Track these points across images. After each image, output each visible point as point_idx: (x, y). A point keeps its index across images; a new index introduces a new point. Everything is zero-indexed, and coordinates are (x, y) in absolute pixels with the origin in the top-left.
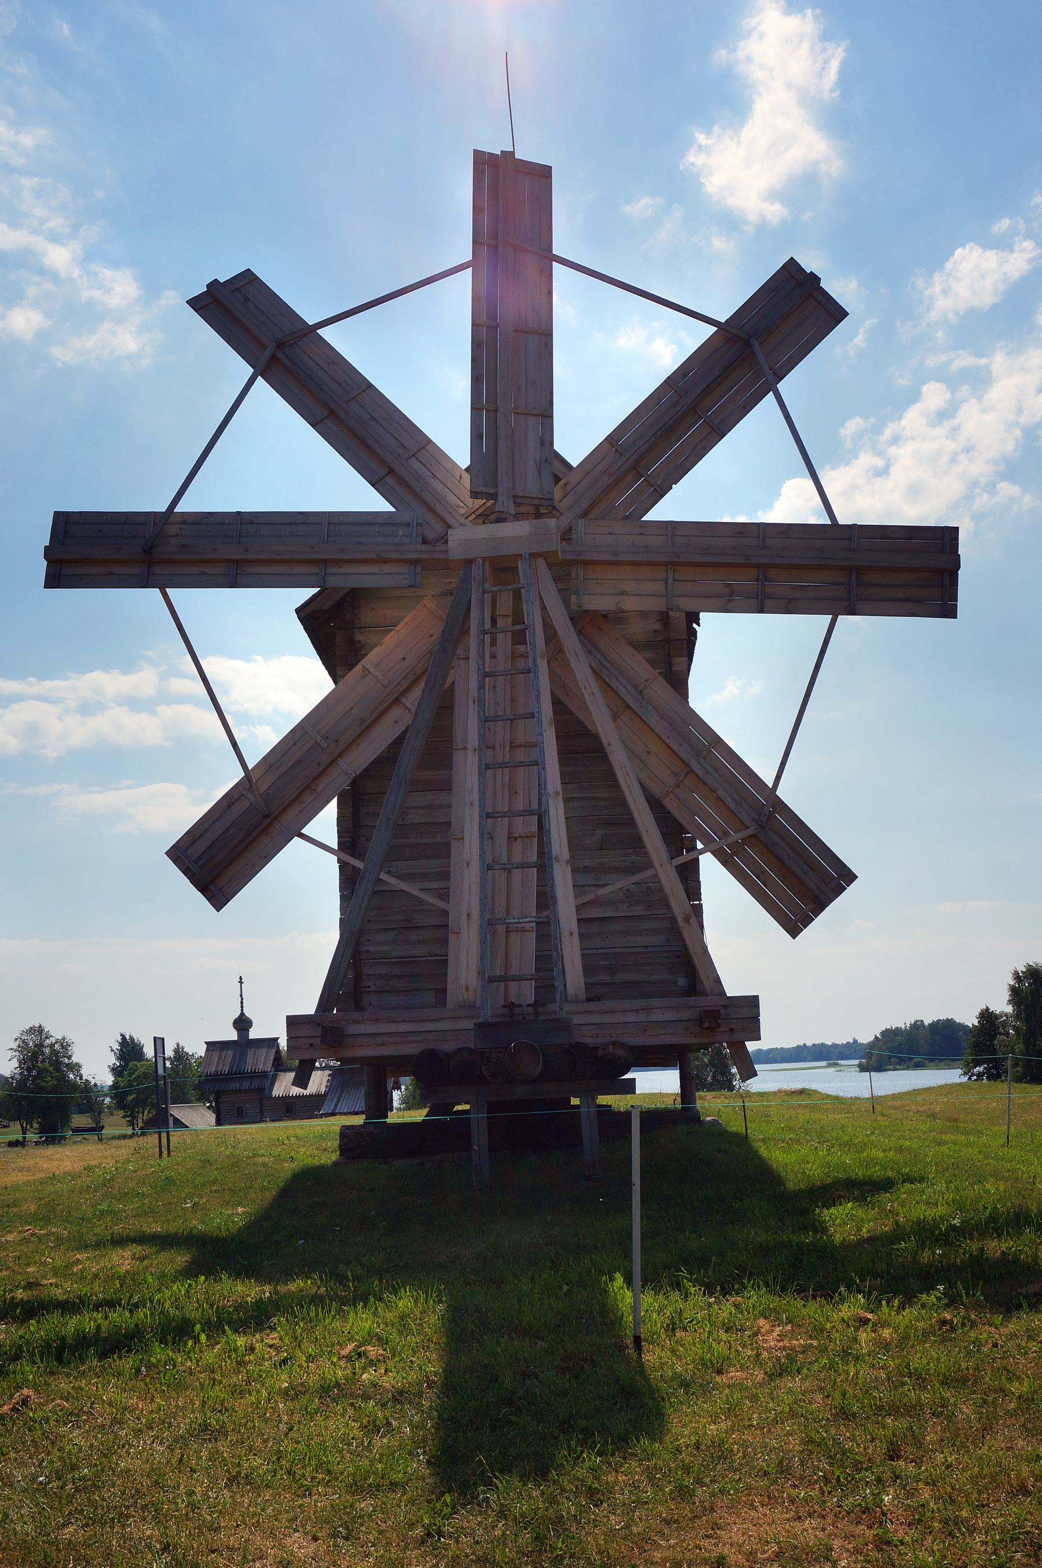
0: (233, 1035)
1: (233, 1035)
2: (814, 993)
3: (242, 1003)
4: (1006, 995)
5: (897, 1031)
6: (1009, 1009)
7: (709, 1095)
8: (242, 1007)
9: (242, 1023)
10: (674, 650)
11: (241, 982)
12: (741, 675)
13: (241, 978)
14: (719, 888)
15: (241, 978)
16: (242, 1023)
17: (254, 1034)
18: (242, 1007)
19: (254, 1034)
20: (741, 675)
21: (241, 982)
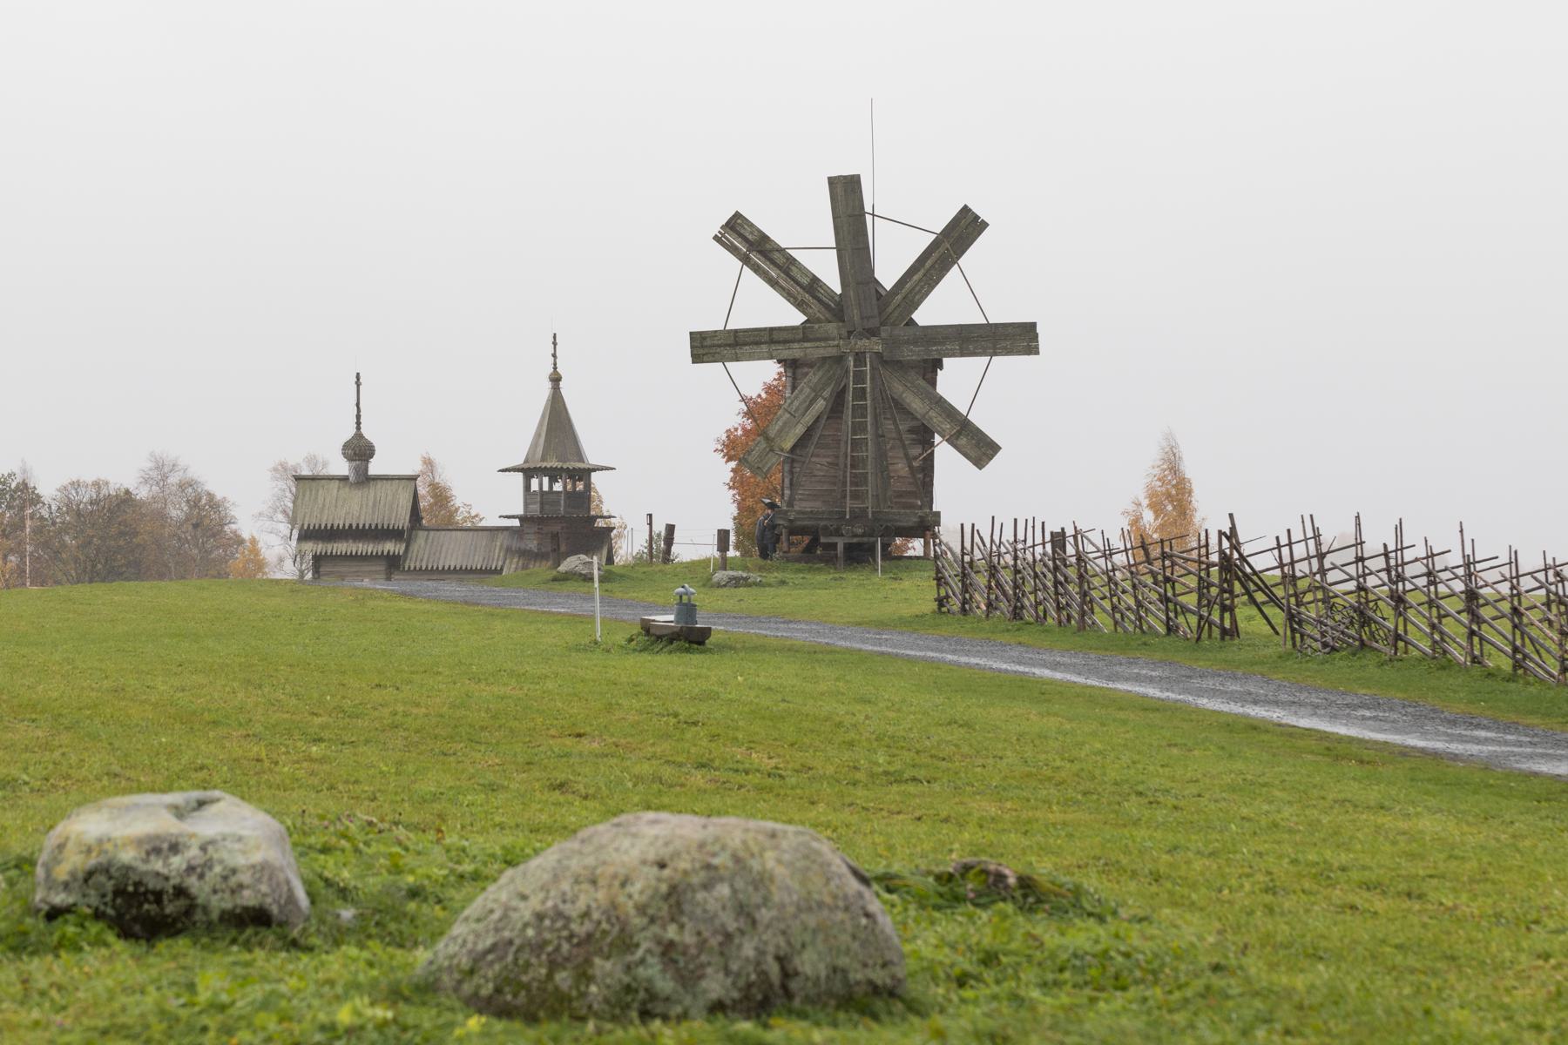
1: (341, 467)
2: (964, 499)
3: (358, 417)
8: (358, 423)
9: (359, 450)
10: (912, 323)
14: (946, 457)
16: (359, 450)
17: (375, 467)
18: (358, 423)
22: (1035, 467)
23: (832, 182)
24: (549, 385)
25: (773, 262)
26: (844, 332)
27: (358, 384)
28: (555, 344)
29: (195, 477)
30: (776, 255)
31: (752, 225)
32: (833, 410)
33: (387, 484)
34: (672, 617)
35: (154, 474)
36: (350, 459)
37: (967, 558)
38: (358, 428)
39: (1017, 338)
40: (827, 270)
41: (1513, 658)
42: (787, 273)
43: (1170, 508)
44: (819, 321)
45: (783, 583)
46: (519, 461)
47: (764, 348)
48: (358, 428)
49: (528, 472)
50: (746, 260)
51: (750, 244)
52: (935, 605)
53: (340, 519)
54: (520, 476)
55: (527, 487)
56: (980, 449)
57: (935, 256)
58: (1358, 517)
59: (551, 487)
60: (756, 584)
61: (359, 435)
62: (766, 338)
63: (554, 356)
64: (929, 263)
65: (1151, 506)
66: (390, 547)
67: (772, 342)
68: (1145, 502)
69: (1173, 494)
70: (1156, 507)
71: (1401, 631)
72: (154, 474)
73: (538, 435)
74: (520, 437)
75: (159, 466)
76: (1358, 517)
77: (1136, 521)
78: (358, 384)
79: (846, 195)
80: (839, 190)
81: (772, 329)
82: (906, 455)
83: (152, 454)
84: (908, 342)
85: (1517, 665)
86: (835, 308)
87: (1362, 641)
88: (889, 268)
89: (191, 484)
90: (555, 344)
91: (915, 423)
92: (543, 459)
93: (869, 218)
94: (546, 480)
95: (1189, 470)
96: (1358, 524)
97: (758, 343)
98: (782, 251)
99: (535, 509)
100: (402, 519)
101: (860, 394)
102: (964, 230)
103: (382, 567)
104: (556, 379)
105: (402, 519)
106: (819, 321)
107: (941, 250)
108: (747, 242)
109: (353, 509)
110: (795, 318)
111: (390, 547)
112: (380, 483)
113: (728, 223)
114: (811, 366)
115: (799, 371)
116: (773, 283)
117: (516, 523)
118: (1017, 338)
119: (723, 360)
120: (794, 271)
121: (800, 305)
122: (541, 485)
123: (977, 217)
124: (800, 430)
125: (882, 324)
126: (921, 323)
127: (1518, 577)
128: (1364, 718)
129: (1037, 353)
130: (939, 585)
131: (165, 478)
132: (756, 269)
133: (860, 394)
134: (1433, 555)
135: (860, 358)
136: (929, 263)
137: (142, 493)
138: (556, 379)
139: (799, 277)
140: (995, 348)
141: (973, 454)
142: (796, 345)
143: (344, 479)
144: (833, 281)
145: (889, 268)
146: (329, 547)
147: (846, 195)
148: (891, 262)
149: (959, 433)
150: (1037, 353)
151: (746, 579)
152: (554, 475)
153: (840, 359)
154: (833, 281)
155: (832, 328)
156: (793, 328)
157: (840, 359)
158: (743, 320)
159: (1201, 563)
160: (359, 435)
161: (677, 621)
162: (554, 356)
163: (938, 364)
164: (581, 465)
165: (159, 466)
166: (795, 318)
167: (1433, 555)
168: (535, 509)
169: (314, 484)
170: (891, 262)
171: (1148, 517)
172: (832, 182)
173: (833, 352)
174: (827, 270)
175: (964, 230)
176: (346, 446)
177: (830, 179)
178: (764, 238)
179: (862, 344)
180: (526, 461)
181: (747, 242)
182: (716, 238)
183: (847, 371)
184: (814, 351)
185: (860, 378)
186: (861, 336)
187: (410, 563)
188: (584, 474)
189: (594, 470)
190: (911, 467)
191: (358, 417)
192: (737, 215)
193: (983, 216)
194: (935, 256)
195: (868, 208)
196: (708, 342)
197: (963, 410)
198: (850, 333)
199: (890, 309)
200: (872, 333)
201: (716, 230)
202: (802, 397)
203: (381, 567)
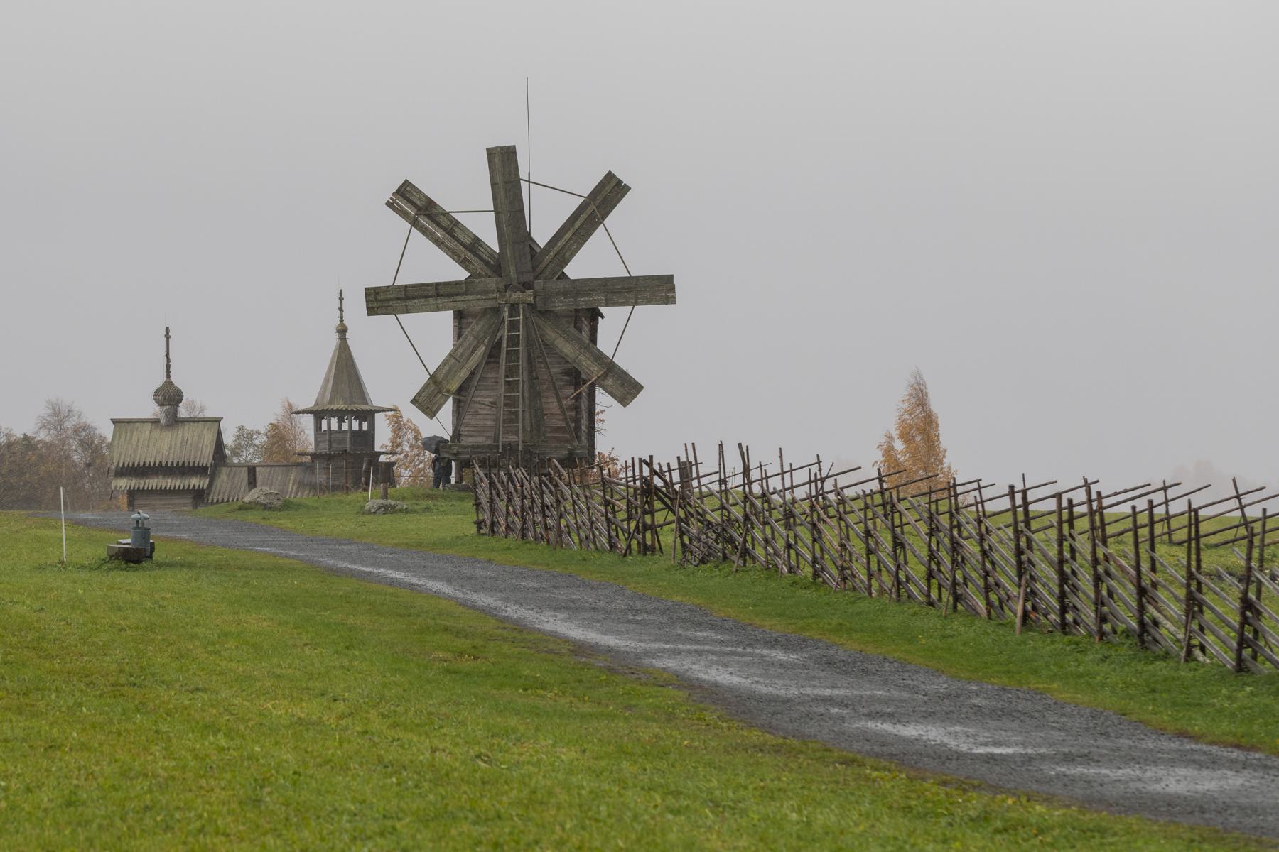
2: (625, 436)
3: (168, 366)
8: (168, 372)
9: (169, 396)
10: (564, 276)
14: (603, 399)
16: (169, 396)
17: (183, 412)
18: (168, 372)
22: (672, 405)
23: (490, 152)
24: (337, 336)
25: (438, 224)
26: (502, 285)
27: (168, 337)
28: (341, 299)
29: (89, 422)
30: (441, 219)
31: (420, 192)
32: (490, 356)
33: (194, 427)
34: (129, 541)
35: (52, 419)
36: (161, 404)
37: (756, 489)
38: (168, 376)
39: (658, 289)
40: (486, 230)
41: (813, 566)
42: (450, 233)
43: (918, 439)
44: (480, 276)
45: (428, 509)
46: (310, 403)
47: (431, 300)
48: (168, 376)
50: (415, 223)
51: (419, 210)
52: (474, 529)
53: (151, 458)
54: (311, 417)
55: (318, 427)
56: (627, 389)
57: (583, 217)
58: (721, 445)
59: (340, 427)
60: (407, 511)
61: (168, 384)
62: (432, 292)
63: (341, 309)
64: (577, 225)
65: (901, 436)
66: (195, 482)
67: (438, 295)
68: (895, 434)
69: (921, 428)
70: (906, 436)
71: (749, 546)
72: (52, 419)
73: (327, 380)
74: (308, 384)
75: (56, 413)
76: (721, 445)
77: (888, 451)
78: (168, 337)
79: (503, 162)
80: (497, 160)
81: (438, 284)
82: (557, 394)
83: (49, 402)
84: (558, 294)
85: (816, 575)
86: (496, 266)
87: (724, 554)
88: (543, 228)
89: (85, 428)
90: (341, 299)
91: (569, 366)
92: (331, 402)
93: (524, 185)
94: (334, 421)
95: (936, 406)
96: (721, 452)
97: (426, 297)
98: (446, 214)
99: (324, 446)
100: (206, 457)
101: (514, 341)
102: (609, 193)
103: (188, 500)
104: (342, 331)
105: (206, 457)
106: (480, 276)
107: (589, 211)
108: (415, 206)
109: (164, 447)
110: (460, 274)
111: (195, 482)
112: (187, 425)
113: (398, 191)
114: (474, 316)
115: (464, 321)
116: (439, 243)
117: (307, 459)
118: (658, 289)
119: (394, 311)
120: (458, 233)
121: (464, 263)
122: (350, 426)
123: (620, 182)
124: (464, 374)
125: (537, 278)
127: (982, 502)
128: (644, 624)
129: (674, 302)
130: (477, 510)
131: (61, 423)
132: (424, 231)
133: (514, 341)
134: (767, 477)
135: (514, 308)
136: (577, 225)
137: (42, 436)
138: (342, 331)
139: (462, 237)
140: (636, 298)
141: (617, 393)
142: (459, 298)
143: (155, 422)
144: (491, 240)
145: (543, 228)
146: (142, 482)
147: (503, 162)
148: (543, 224)
149: (605, 376)
150: (674, 302)
151: (394, 507)
152: (341, 415)
153: (496, 311)
154: (491, 240)
155: (492, 283)
156: (457, 283)
157: (496, 311)
158: (412, 276)
159: (628, 487)
160: (168, 384)
161: (134, 542)
162: (341, 309)
163: (595, 315)
164: (364, 407)
165: (56, 413)
166: (460, 274)
167: (767, 477)
168: (324, 446)
169: (129, 427)
170: (543, 224)
171: (899, 446)
172: (490, 152)
173: (489, 304)
174: (486, 230)
175: (609, 193)
176: (157, 393)
177: (488, 150)
178: (431, 203)
179: (515, 296)
180: (316, 404)
181: (415, 206)
182: (388, 204)
183: (503, 321)
184: (475, 304)
185: (513, 326)
186: (515, 289)
187: (214, 497)
188: (368, 415)
189: (379, 411)
190: (561, 406)
191: (168, 366)
192: (407, 183)
193: (626, 181)
194: (583, 217)
195: (523, 174)
196: (381, 297)
197: (609, 353)
198: (507, 287)
199: (543, 265)
200: (527, 286)
201: (388, 196)
202: (466, 344)
203: (188, 500)
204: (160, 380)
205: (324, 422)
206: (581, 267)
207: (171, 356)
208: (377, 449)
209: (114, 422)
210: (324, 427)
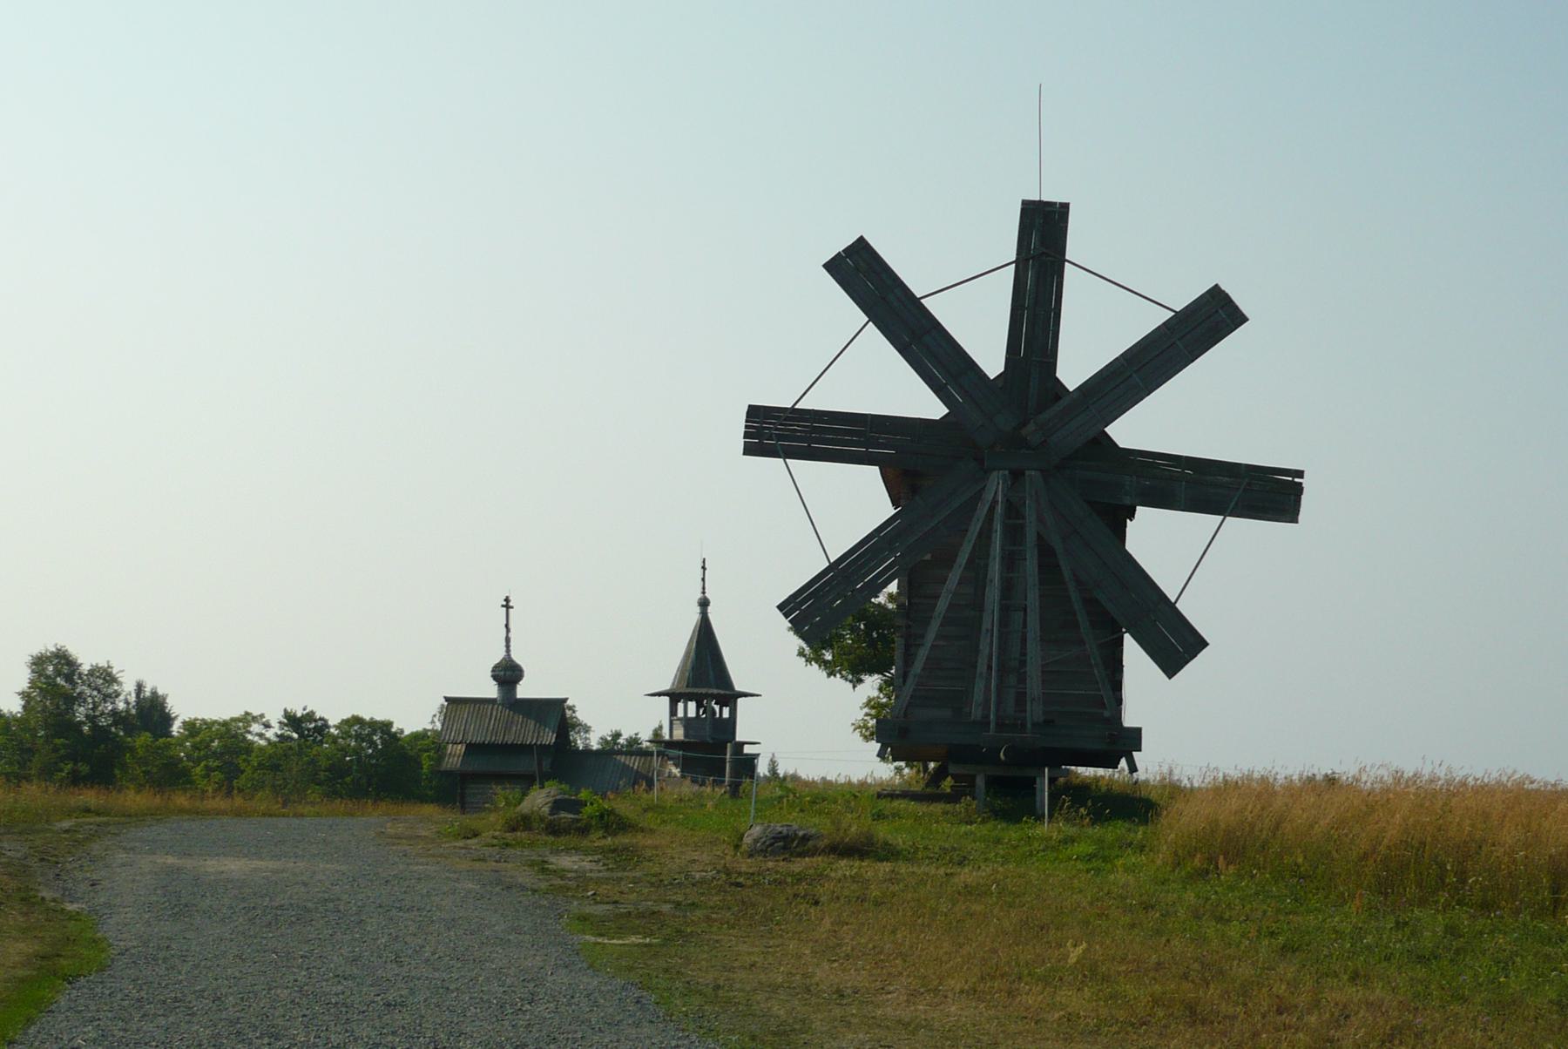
0: (491, 690)
1: (491, 690)
2: (1177, 727)
3: (508, 640)
4: (839, 684)
5: (1352, 787)
6: (871, 685)
7: (844, 536)
8: (508, 646)
9: (508, 674)
10: (1118, 518)
11: (507, 605)
12: (1159, 540)
13: (507, 600)
14: (1133, 653)
15: (507, 600)
16: (508, 674)
17: (524, 691)
18: (508, 646)
19: (524, 691)
20: (1159, 540)
21: (507, 605)
22: (1259, 683)
24: (698, 609)
46: (667, 686)
49: (674, 697)
55: (673, 712)
56: (1176, 644)
94: (692, 706)
102: (862, 273)
104: (704, 604)
126: (1132, 546)
138: (704, 604)
148: (983, 333)
170: (983, 333)
175: (862, 273)
191: (508, 640)
193: (780, 615)
204: (498, 656)
205: (680, 706)
206: (1132, 430)
207: (511, 626)
208: (739, 738)
209: (447, 699)
210: (680, 714)
